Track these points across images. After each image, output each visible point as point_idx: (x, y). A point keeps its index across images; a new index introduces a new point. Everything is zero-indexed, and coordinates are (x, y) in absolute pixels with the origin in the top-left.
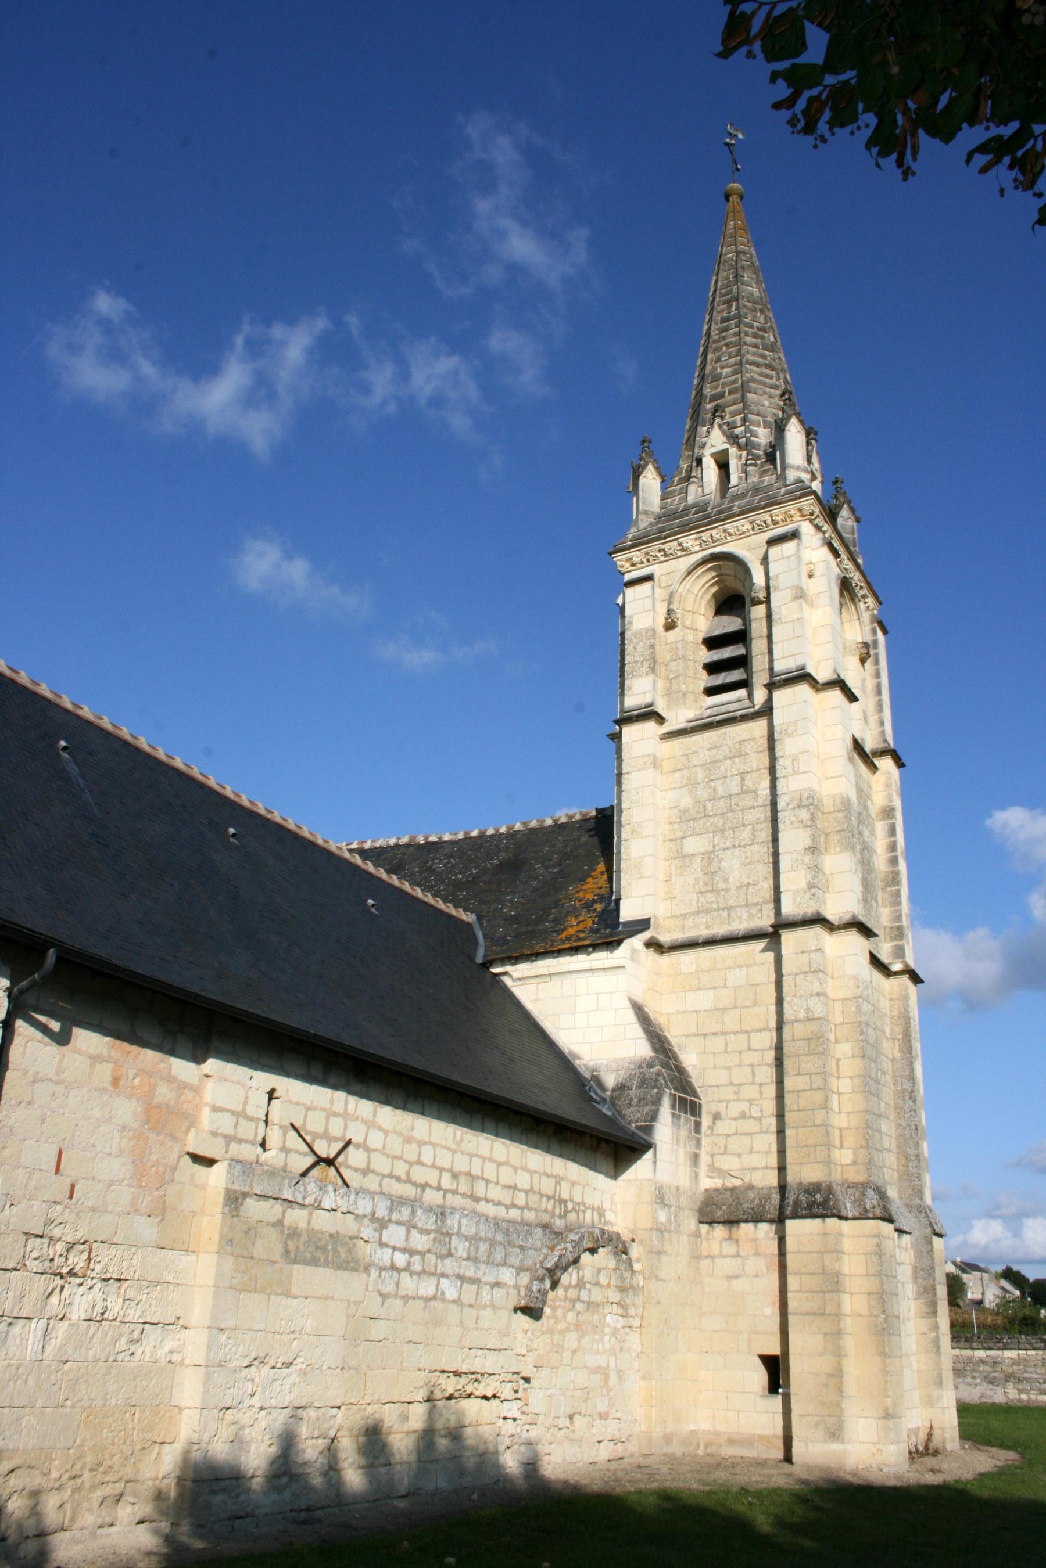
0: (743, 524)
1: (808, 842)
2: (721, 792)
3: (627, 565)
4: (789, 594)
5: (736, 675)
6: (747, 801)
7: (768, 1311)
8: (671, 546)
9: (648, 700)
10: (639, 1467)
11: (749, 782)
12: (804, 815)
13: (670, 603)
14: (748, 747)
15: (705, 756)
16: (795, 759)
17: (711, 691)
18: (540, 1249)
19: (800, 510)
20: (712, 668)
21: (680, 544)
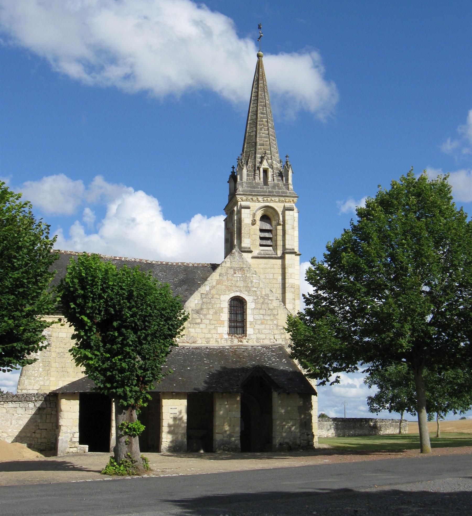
0: (277, 199)
1: (293, 297)
2: (267, 277)
3: (240, 200)
4: (291, 227)
5: (269, 242)
6: (275, 281)
7: (191, 463)
8: (255, 198)
9: (249, 246)
10: (288, 394)
11: (275, 276)
12: (293, 290)
13: (254, 217)
14: (275, 266)
15: (262, 266)
16: (291, 274)
17: (261, 245)
18: (461, 285)
19: (293, 200)
20: (261, 238)
21: (257, 199)
